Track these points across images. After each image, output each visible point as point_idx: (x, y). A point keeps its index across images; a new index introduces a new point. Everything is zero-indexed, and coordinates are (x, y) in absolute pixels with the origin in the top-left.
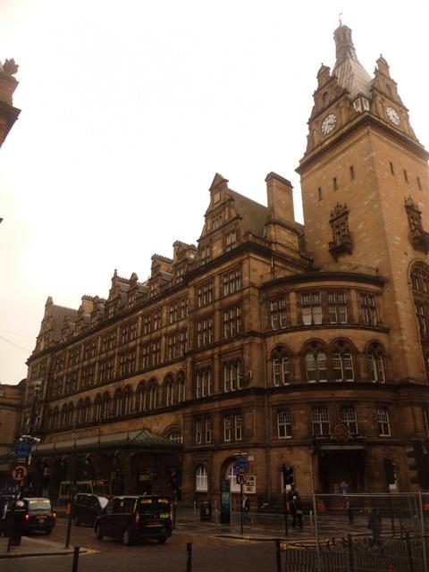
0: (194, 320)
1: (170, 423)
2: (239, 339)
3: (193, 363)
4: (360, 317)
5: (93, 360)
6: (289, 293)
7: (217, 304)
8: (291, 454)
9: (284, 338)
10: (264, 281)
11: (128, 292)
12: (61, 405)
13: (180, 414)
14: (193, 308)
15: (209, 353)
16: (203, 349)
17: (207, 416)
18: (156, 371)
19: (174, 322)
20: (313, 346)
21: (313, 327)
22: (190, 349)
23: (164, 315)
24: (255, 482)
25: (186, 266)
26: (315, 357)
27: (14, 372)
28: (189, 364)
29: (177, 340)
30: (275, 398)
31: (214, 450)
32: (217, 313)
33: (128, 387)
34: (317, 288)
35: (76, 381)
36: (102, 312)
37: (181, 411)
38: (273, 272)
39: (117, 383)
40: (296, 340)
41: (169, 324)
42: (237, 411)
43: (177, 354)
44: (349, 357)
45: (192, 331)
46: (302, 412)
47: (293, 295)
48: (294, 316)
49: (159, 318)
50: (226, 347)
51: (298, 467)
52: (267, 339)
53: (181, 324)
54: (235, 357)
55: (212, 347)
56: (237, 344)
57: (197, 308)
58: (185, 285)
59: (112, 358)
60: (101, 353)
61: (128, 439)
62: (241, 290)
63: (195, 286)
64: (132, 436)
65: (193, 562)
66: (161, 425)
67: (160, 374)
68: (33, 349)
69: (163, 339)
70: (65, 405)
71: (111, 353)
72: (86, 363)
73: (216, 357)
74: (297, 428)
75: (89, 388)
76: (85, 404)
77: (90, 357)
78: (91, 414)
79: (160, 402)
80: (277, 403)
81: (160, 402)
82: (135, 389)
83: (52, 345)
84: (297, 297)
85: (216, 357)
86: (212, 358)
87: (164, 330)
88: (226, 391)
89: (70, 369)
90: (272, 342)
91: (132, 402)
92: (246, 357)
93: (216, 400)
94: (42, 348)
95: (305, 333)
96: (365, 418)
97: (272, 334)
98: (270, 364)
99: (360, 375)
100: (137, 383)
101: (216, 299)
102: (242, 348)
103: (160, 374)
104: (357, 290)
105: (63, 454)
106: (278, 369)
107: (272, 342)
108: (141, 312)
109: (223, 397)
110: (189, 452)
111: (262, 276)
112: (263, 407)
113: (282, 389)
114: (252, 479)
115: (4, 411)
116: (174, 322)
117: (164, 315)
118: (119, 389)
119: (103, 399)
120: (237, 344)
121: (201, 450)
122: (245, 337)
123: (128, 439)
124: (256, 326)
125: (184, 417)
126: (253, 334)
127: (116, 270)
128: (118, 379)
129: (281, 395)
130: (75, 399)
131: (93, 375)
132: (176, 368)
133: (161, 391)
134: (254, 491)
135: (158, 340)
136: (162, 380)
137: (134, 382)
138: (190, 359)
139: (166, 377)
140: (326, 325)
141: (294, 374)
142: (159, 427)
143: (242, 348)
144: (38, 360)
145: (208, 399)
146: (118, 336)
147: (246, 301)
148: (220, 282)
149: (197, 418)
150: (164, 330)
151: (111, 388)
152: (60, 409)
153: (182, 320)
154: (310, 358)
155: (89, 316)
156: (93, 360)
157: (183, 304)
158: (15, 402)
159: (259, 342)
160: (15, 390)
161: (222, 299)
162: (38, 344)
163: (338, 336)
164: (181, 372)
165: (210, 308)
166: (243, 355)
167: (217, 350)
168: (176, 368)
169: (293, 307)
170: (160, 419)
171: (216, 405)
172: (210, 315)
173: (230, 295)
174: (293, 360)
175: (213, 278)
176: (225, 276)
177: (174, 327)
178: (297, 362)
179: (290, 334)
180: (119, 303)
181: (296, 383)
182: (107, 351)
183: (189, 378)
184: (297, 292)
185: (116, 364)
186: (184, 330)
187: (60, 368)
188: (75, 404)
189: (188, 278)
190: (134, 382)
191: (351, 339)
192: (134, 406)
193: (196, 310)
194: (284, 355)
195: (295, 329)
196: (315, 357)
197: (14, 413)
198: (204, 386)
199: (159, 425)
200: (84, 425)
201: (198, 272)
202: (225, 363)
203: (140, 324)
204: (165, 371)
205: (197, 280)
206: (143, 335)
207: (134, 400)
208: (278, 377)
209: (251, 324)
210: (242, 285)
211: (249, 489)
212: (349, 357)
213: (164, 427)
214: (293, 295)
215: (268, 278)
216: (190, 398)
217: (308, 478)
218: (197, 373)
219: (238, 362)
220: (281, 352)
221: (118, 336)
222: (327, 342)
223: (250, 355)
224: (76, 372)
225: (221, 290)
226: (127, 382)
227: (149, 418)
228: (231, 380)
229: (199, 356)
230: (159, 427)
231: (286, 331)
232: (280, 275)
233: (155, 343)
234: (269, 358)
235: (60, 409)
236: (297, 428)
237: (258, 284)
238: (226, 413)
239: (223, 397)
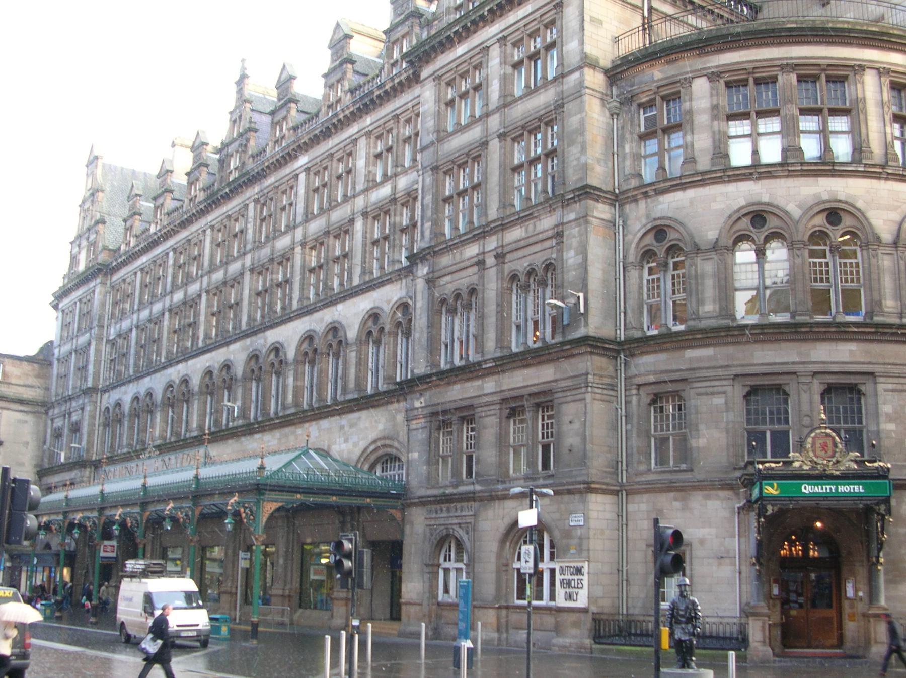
0: (435, 169)
1: (372, 436)
2: (552, 210)
3: (431, 282)
4: (887, 147)
5: (194, 288)
6: (689, 81)
7: (494, 122)
8: (685, 508)
9: (670, 204)
10: (623, 52)
11: (272, 113)
12: (127, 399)
13: (397, 411)
14: (432, 137)
15: (472, 250)
16: (460, 242)
17: (467, 415)
18: (340, 307)
19: (386, 178)
20: (758, 223)
21: (757, 171)
22: (424, 245)
23: (361, 163)
24: (585, 578)
25: (417, 29)
26: (760, 253)
27: (32, 327)
28: (420, 284)
29: (393, 226)
30: (649, 364)
31: (481, 500)
32: (495, 145)
33: (277, 349)
34: (770, 64)
35: (159, 339)
36: (214, 168)
37: (402, 405)
38: (647, 26)
39: (248, 341)
40: (706, 210)
41: (372, 185)
42: (544, 401)
43: (393, 262)
44: (854, 254)
45: (429, 199)
46: (719, 401)
47: (701, 86)
48: (702, 142)
49: (349, 172)
50: (515, 234)
51: (702, 542)
52: (627, 208)
53: (403, 182)
54: (538, 260)
55: (480, 234)
56: (547, 222)
57: (442, 136)
58: (414, 79)
59: (237, 280)
60: (212, 269)
61: (262, 468)
62: (561, 76)
63: (437, 77)
64: (273, 464)
65: (526, 662)
66: (355, 439)
67: (351, 314)
68: (65, 270)
69: (359, 225)
70: (136, 398)
71: (234, 268)
72: (178, 296)
73: (490, 261)
74: (702, 442)
75: (187, 356)
76: (177, 396)
77: (189, 279)
78: (195, 417)
79: (352, 385)
80: (652, 379)
81: (352, 385)
82: (291, 354)
83: (102, 257)
84: (714, 93)
85: (490, 261)
86: (480, 263)
87: (360, 202)
88: (515, 349)
89: (145, 314)
90: (639, 216)
91: (285, 386)
92: (571, 257)
93: (490, 372)
94: (81, 267)
95: (731, 188)
96: (890, 418)
97: (648, 191)
98: (634, 274)
99: (880, 304)
100: (296, 339)
101: (492, 107)
102: (559, 235)
103: (351, 314)
104: (882, 71)
105: (231, 493)
106: (654, 286)
107: (639, 216)
108: (303, 160)
109: (509, 362)
110: (423, 502)
111: (616, 40)
112: (613, 387)
113: (667, 341)
114: (579, 571)
115: (5, 412)
116: (386, 178)
117: (361, 163)
118: (254, 357)
119: (219, 383)
120: (547, 222)
121: (447, 500)
122: (565, 203)
123: (262, 468)
124: (598, 177)
125: (408, 420)
126: (586, 192)
127: (243, 61)
128: (254, 331)
129: (662, 357)
130: (156, 383)
131: (194, 325)
132: (387, 297)
133: (352, 356)
134: (582, 601)
135: (344, 230)
136: (357, 327)
137: (289, 335)
138: (423, 270)
139: (364, 322)
140: (792, 165)
141: (700, 302)
142: (350, 445)
143: (559, 235)
144: (75, 295)
145: (469, 371)
146: (250, 228)
147: (569, 107)
148: (504, 63)
149: (442, 420)
150: (360, 202)
151: (237, 354)
152: (126, 408)
153: (405, 172)
154: (745, 255)
155: (183, 180)
156: (194, 288)
157: (408, 131)
158: (28, 394)
159: (607, 216)
160: (26, 367)
161: (505, 106)
162: (74, 259)
163: (825, 197)
164: (404, 306)
165: (475, 133)
166: (560, 251)
167: (492, 243)
168: (387, 297)
169: (702, 119)
170: (352, 426)
171: (489, 385)
172: (475, 155)
173: (530, 92)
174: (698, 260)
175: (485, 50)
176: (516, 44)
177: (385, 191)
178: (707, 267)
179: (691, 193)
180: (252, 143)
181: (703, 324)
182: (225, 264)
183: (420, 321)
184: (713, 77)
185: (246, 292)
186: (410, 197)
187: (123, 312)
188: (158, 396)
189: (420, 57)
190: (289, 335)
191: (860, 204)
192: (290, 397)
193: (440, 140)
194: (674, 249)
195: (703, 179)
196: (760, 253)
197: (29, 418)
198: (458, 339)
199: (344, 443)
200: (177, 444)
201: (444, 43)
202: (514, 277)
203: (301, 190)
204: (363, 304)
205: (443, 60)
206: (308, 217)
207: (290, 380)
208: (654, 313)
209: (585, 168)
210: (561, 64)
211: (569, 597)
212: (854, 254)
213: (362, 445)
214: (701, 86)
215: (635, 43)
216: (421, 369)
217: (727, 571)
218: (449, 305)
219: (545, 275)
220: (665, 246)
221: (250, 228)
222: (795, 211)
223: (583, 251)
224: (156, 320)
225: (506, 81)
226: (273, 336)
227: (325, 423)
228: (527, 321)
229: (445, 260)
230: (350, 445)
231: (681, 185)
232: (667, 32)
233: (337, 237)
234: (631, 258)
235: (126, 408)
236: (702, 442)
237: (606, 62)
238: (513, 407)
239: (509, 362)
